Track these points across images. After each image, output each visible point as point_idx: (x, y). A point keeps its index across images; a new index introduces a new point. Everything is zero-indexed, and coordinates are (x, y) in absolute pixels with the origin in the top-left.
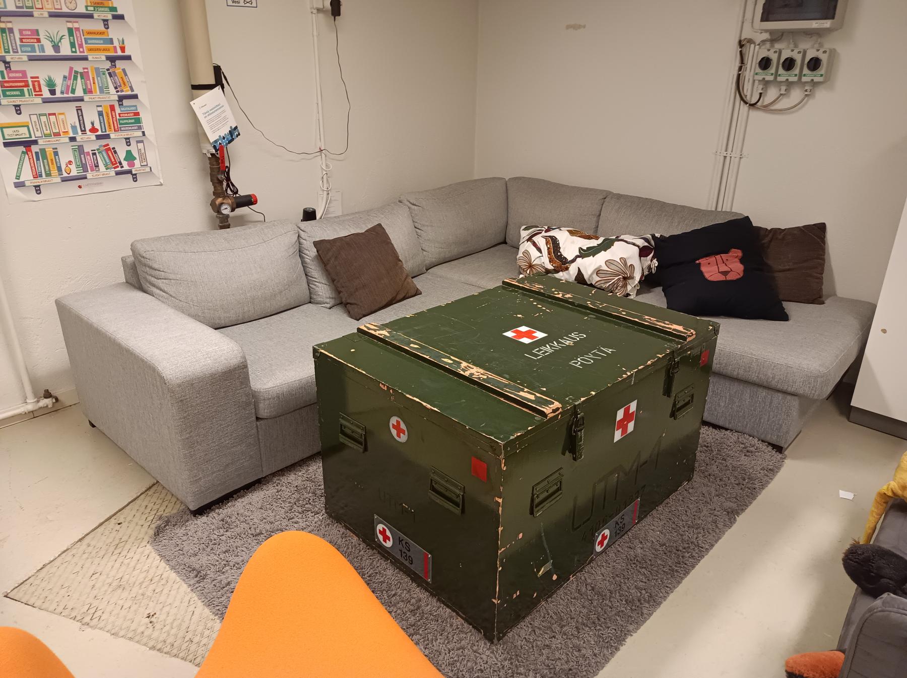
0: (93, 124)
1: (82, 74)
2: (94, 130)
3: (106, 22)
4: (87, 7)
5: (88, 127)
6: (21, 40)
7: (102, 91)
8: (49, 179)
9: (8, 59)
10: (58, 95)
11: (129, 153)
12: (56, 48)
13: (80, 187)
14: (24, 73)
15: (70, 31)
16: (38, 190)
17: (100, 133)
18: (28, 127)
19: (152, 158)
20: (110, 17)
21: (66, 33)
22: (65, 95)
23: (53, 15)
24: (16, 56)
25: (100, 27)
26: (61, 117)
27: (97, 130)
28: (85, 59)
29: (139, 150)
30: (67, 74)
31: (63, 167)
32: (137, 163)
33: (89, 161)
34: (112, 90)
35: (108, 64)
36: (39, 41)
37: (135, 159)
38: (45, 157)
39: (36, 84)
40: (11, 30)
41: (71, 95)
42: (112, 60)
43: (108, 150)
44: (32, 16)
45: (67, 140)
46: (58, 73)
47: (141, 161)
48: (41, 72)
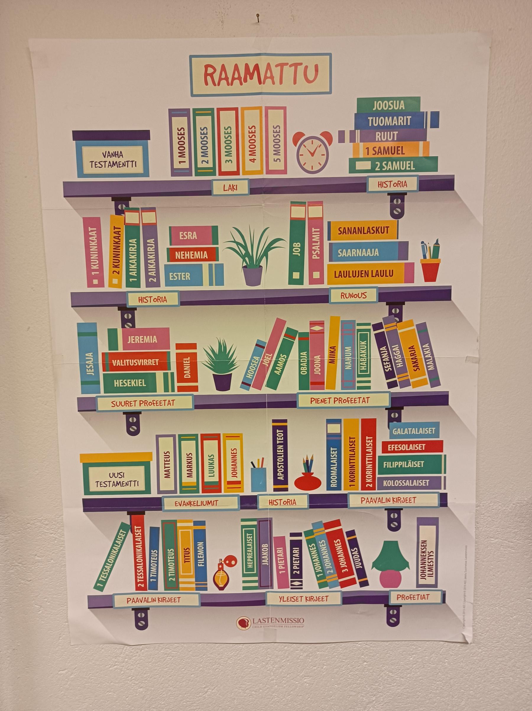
0: (308, 465)
1: (304, 338)
2: (307, 481)
3: (397, 199)
4: (352, 162)
5: (296, 471)
6: (171, 254)
7: (348, 383)
8: (171, 595)
9: (132, 301)
10: (236, 389)
11: (391, 550)
12: (253, 272)
13: (243, 623)
14: (163, 334)
15: (297, 226)
16: (141, 618)
17: (322, 490)
18: (147, 465)
19: (454, 568)
20: (412, 184)
21: (284, 232)
22: (253, 391)
23: (257, 189)
24: (153, 293)
25: (379, 212)
26: (231, 444)
27: (317, 483)
28: (323, 298)
29: (421, 545)
30: (266, 339)
31: (211, 570)
32: (408, 577)
33: (280, 561)
34: (378, 379)
35: (384, 310)
36: (213, 255)
37: (406, 565)
38: (171, 541)
39: (187, 362)
40: (151, 230)
41: (266, 390)
42: (394, 300)
43: (331, 537)
44: (209, 193)
45: (235, 503)
46: (242, 335)
47: (421, 574)
48: (203, 332)
